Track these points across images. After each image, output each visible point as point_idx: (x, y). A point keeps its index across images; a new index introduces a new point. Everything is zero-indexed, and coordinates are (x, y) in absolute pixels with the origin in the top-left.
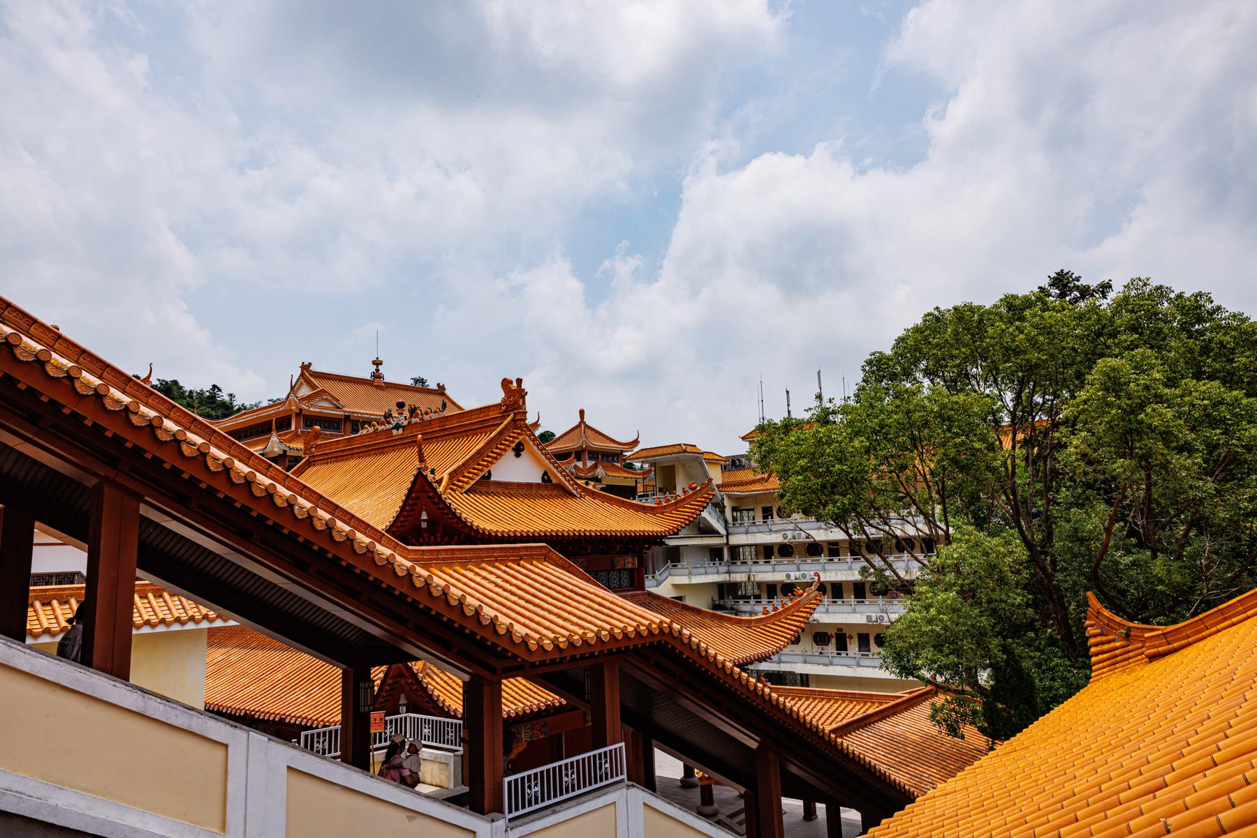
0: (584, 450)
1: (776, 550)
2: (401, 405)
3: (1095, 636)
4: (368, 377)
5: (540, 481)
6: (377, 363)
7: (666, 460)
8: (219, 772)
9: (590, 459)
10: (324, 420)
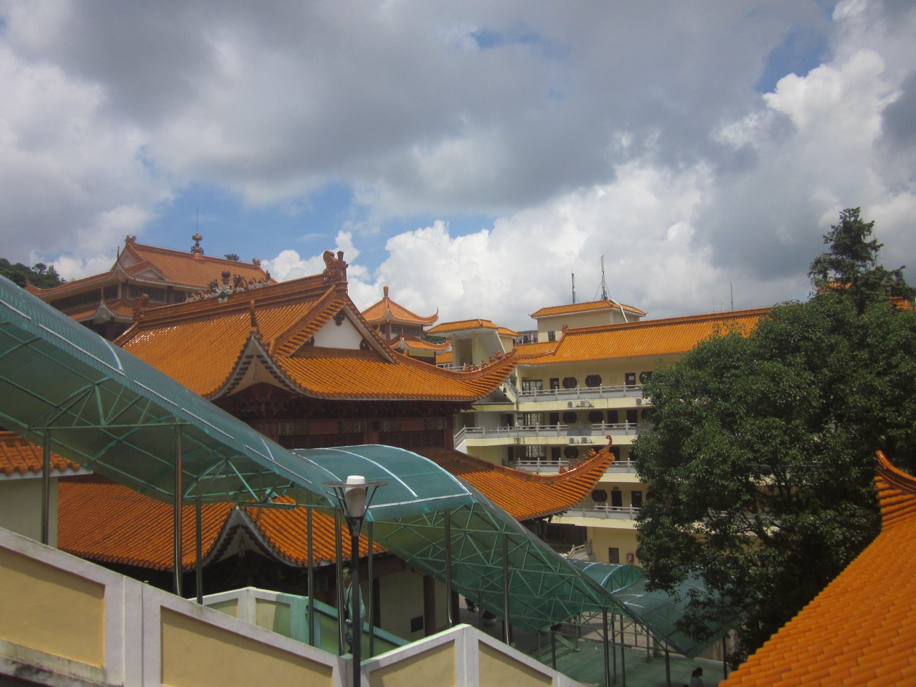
0: (388, 324)
1: (561, 416)
2: (226, 276)
3: (883, 490)
4: (188, 251)
5: (358, 348)
6: (197, 239)
8: (165, 640)
9: (394, 331)
10: (137, 295)
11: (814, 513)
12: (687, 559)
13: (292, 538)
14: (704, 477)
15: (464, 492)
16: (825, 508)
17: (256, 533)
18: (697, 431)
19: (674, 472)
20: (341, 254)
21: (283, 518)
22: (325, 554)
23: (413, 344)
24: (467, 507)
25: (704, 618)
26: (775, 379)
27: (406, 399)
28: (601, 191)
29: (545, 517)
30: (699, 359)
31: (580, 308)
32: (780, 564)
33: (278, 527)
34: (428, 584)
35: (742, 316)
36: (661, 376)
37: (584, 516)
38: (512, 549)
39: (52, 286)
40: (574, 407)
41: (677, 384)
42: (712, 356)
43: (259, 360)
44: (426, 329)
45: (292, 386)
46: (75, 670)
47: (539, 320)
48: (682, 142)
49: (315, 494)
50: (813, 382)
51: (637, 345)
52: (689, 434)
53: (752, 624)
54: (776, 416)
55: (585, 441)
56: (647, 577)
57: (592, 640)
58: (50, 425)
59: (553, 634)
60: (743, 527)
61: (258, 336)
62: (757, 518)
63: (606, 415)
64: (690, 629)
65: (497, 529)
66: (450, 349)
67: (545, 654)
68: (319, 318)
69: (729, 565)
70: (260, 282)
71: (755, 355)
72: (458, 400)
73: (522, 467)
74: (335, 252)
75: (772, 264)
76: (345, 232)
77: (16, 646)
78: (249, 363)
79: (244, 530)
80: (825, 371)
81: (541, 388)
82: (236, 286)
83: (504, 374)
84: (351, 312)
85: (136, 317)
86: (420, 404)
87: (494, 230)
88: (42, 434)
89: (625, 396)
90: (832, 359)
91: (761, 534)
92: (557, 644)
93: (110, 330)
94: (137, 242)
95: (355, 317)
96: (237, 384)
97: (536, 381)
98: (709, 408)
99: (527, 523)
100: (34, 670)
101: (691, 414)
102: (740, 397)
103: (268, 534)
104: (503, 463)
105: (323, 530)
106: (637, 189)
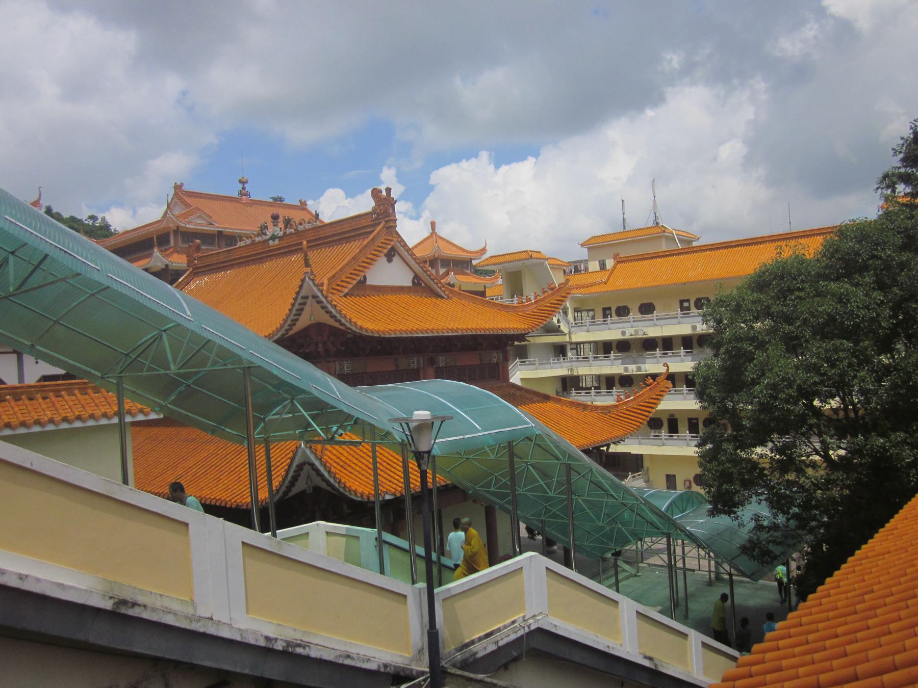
0: (436, 259)
1: (614, 346)
2: (275, 218)
4: (236, 195)
5: (411, 284)
6: (243, 182)
7: (512, 267)
9: (442, 266)
11: (883, 435)
12: (747, 484)
13: (356, 473)
14: (768, 402)
15: (527, 423)
16: (895, 430)
17: (322, 469)
18: (760, 356)
19: (736, 398)
20: (388, 190)
21: (346, 454)
22: (392, 485)
23: (462, 279)
24: (529, 439)
25: (768, 542)
26: (841, 300)
27: (460, 334)
28: (650, 113)
29: (603, 446)
30: (760, 283)
31: (632, 234)
32: (848, 487)
33: (342, 463)
34: (490, 513)
35: (804, 236)
36: (721, 301)
37: (640, 444)
38: (575, 477)
39: (106, 236)
40: (627, 336)
41: (738, 309)
42: (774, 279)
43: (314, 301)
44: (474, 262)
45: (348, 325)
46: (167, 603)
47: (589, 249)
48: (733, 59)
49: (378, 429)
50: (882, 302)
51: (694, 271)
52: (751, 360)
53: (816, 547)
54: (844, 338)
55: (639, 369)
56: (710, 502)
57: (655, 565)
58: (121, 372)
59: (616, 560)
60: (810, 450)
61: (312, 277)
62: (823, 442)
63: (660, 343)
64: (755, 553)
65: (557, 459)
66: (500, 281)
67: (607, 579)
68: (371, 256)
69: (794, 489)
70: (309, 223)
71: (821, 276)
72: (512, 332)
73: (575, 396)
74: (383, 188)
75: (830, 179)
76: (389, 167)
77: (111, 582)
78: (305, 304)
79: (310, 467)
80: (896, 290)
81: (593, 317)
82: (286, 227)
83: (557, 306)
84: (402, 249)
85: (190, 263)
86: (474, 338)
87: (541, 158)
88: (115, 381)
89: (679, 323)
90: (902, 278)
91: (826, 457)
92: (619, 569)
93: (169, 275)
94: (185, 188)
95: (406, 253)
96: (294, 325)
97: (588, 311)
98: (772, 331)
99: (586, 452)
100: (130, 605)
101: (752, 339)
102: (805, 320)
103: (333, 469)
104: (557, 394)
105: (385, 464)
106: (689, 108)
